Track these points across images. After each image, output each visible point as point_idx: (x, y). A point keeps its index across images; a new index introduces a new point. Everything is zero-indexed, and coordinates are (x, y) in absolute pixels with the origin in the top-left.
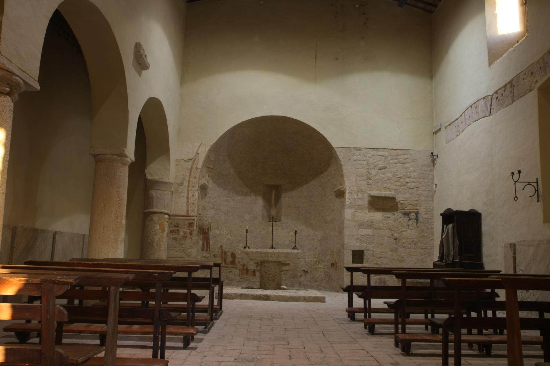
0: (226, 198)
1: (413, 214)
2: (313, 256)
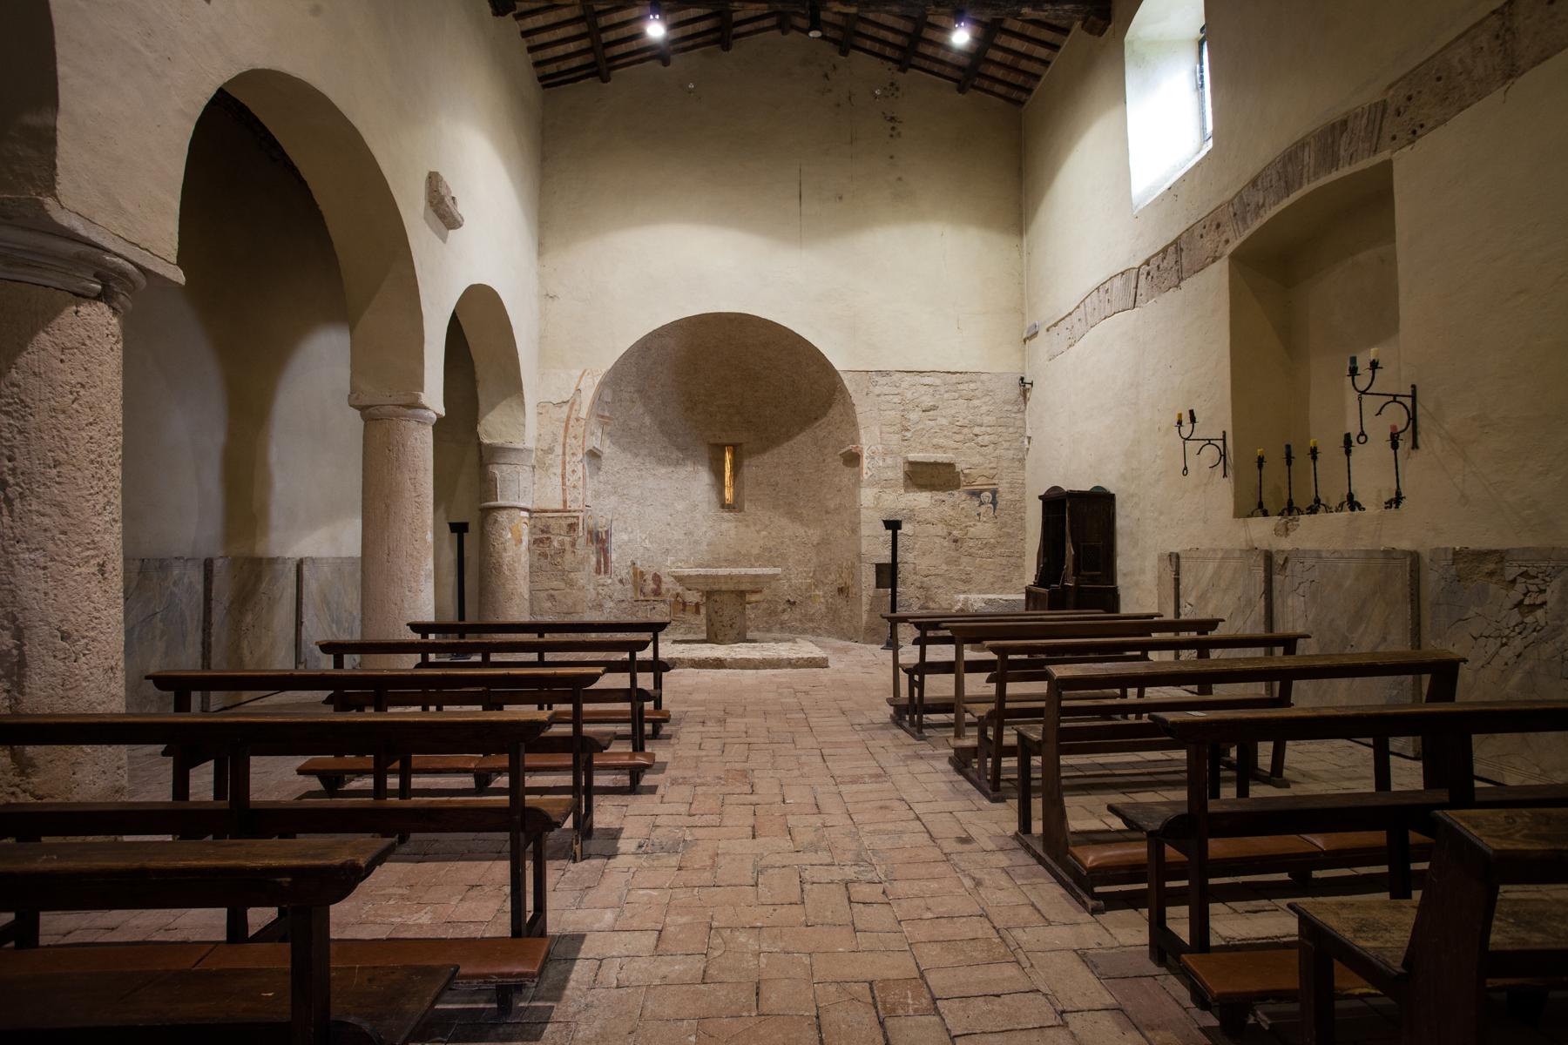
2: (804, 574)
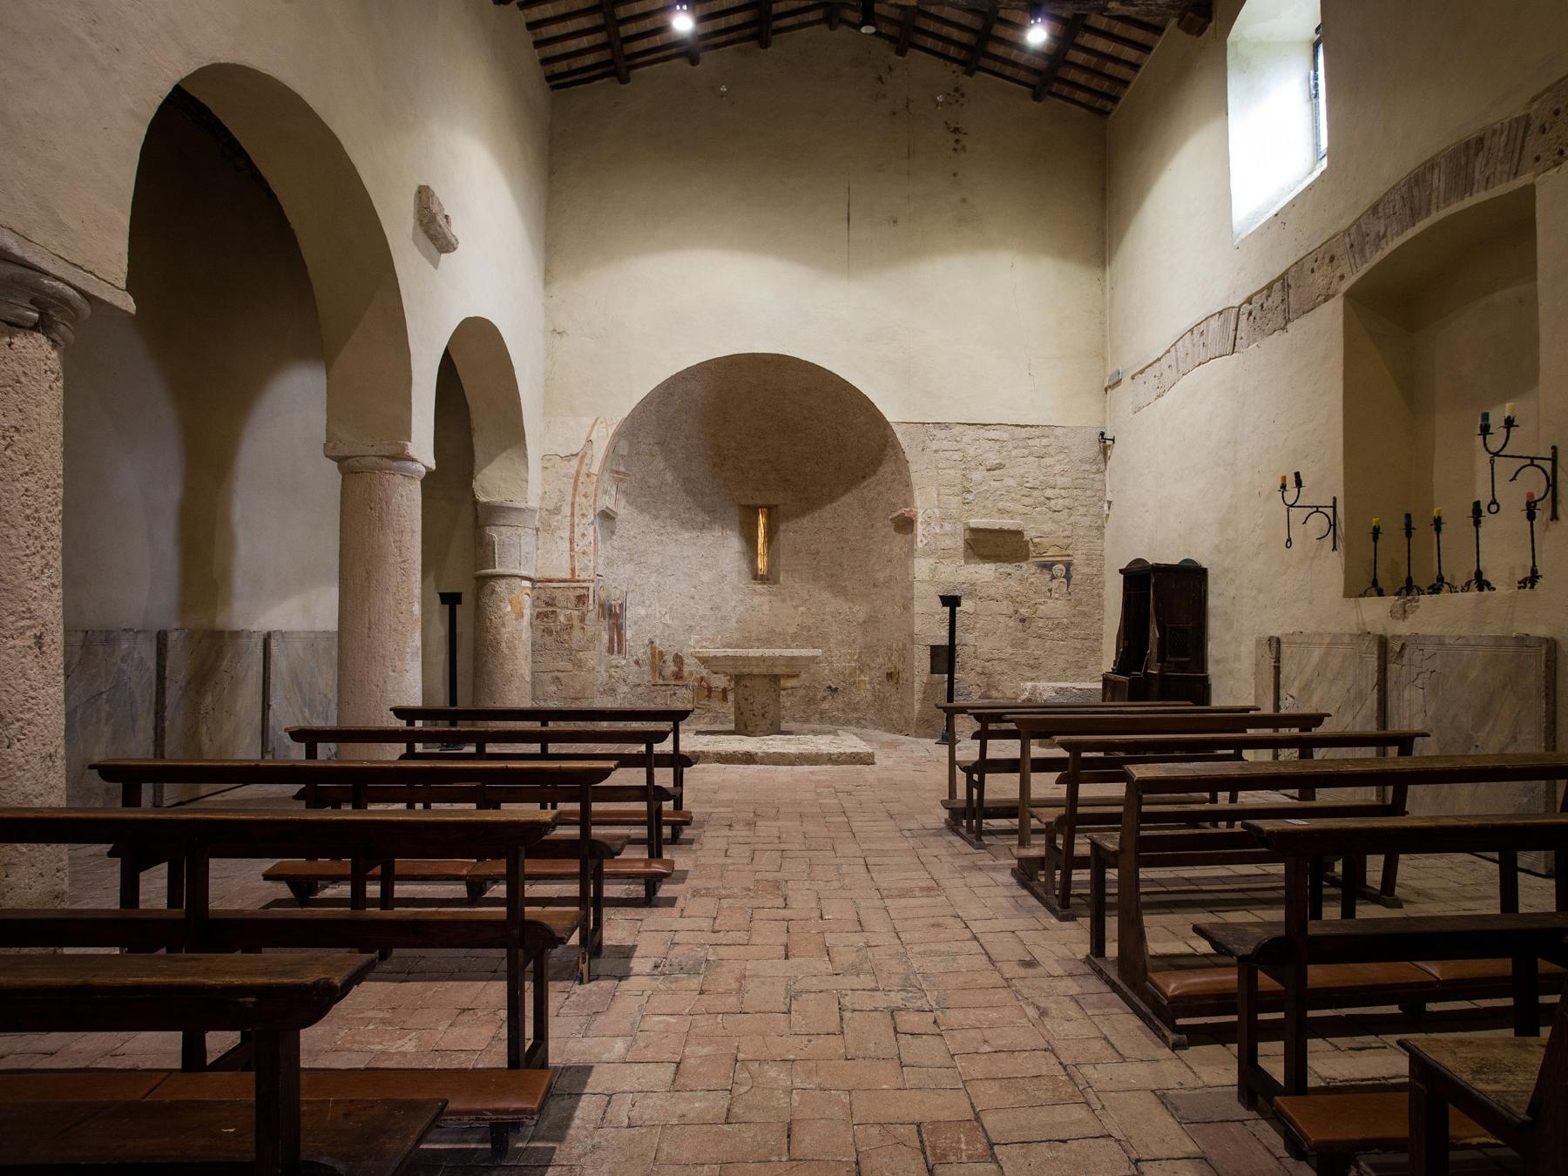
0: (659, 535)
1: (1060, 566)
2: (848, 657)
